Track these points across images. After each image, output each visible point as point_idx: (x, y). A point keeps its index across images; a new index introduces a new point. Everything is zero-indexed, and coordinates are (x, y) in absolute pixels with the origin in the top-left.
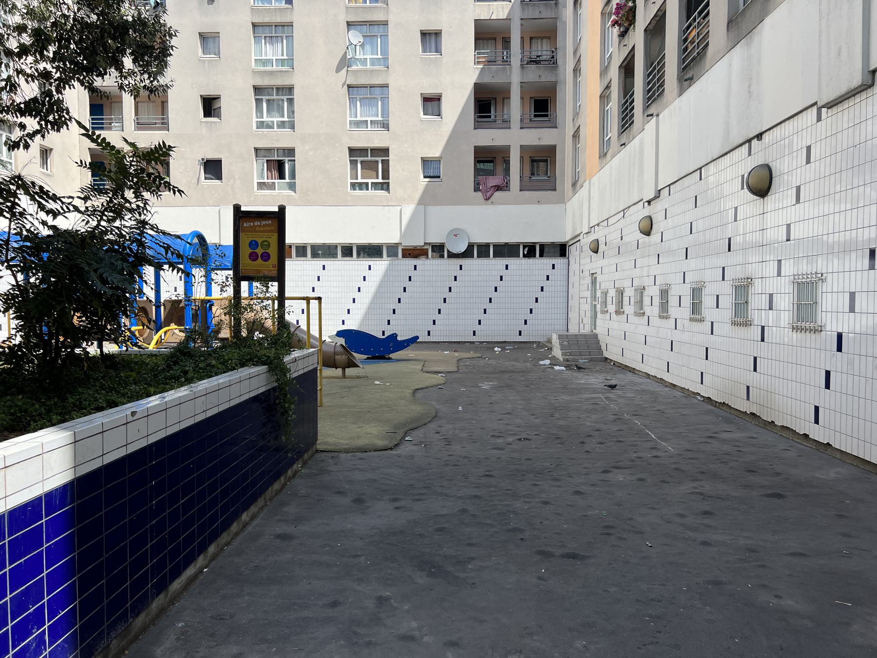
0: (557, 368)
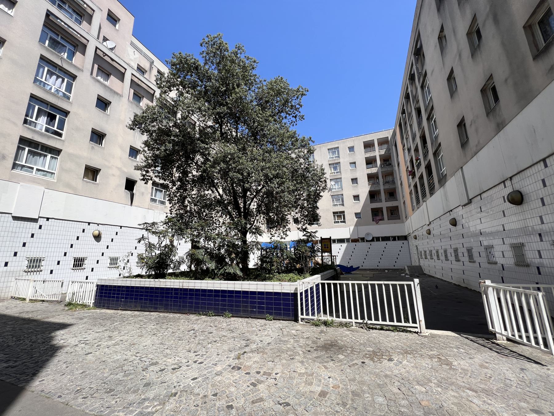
0: (407, 276)
